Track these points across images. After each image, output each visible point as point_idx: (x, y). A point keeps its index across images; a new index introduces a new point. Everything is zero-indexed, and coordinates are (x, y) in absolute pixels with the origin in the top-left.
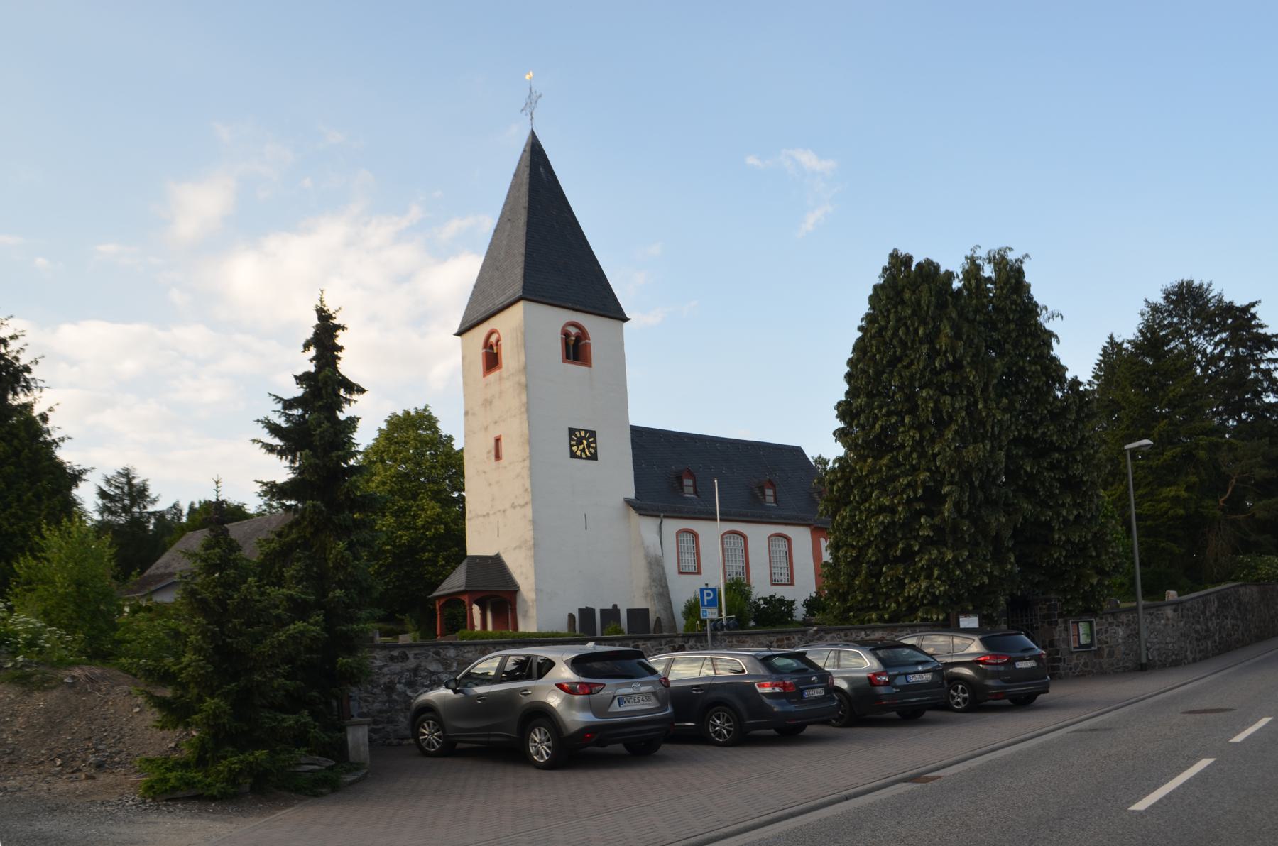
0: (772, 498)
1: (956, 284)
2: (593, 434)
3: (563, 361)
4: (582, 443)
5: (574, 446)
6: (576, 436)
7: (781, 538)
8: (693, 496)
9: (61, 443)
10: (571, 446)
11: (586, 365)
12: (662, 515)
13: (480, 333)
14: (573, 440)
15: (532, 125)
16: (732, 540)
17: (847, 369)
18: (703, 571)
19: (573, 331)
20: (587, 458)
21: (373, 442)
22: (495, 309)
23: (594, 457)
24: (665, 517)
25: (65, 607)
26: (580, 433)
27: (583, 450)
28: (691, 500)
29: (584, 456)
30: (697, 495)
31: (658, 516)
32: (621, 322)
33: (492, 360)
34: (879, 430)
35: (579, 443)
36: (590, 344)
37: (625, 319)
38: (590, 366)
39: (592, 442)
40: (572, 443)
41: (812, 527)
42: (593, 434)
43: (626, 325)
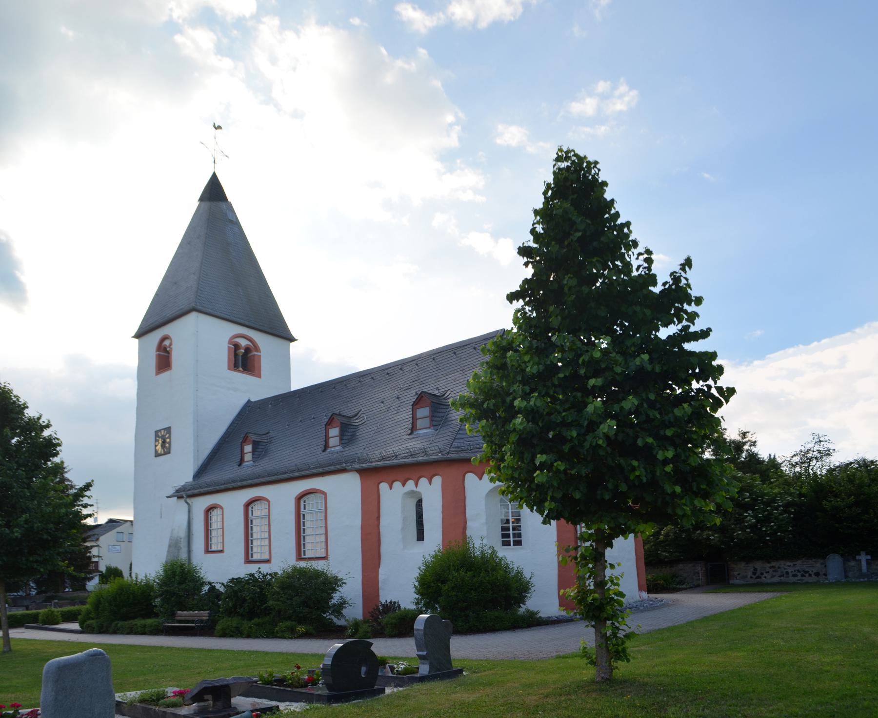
1: (683, 344)
9: (554, 162)
10: (156, 446)
11: (253, 375)
13: (155, 338)
21: (766, 458)
22: (157, 323)
32: (289, 342)
33: (164, 361)
34: (549, 492)
36: (260, 356)
37: (292, 339)
38: (259, 376)
43: (292, 344)
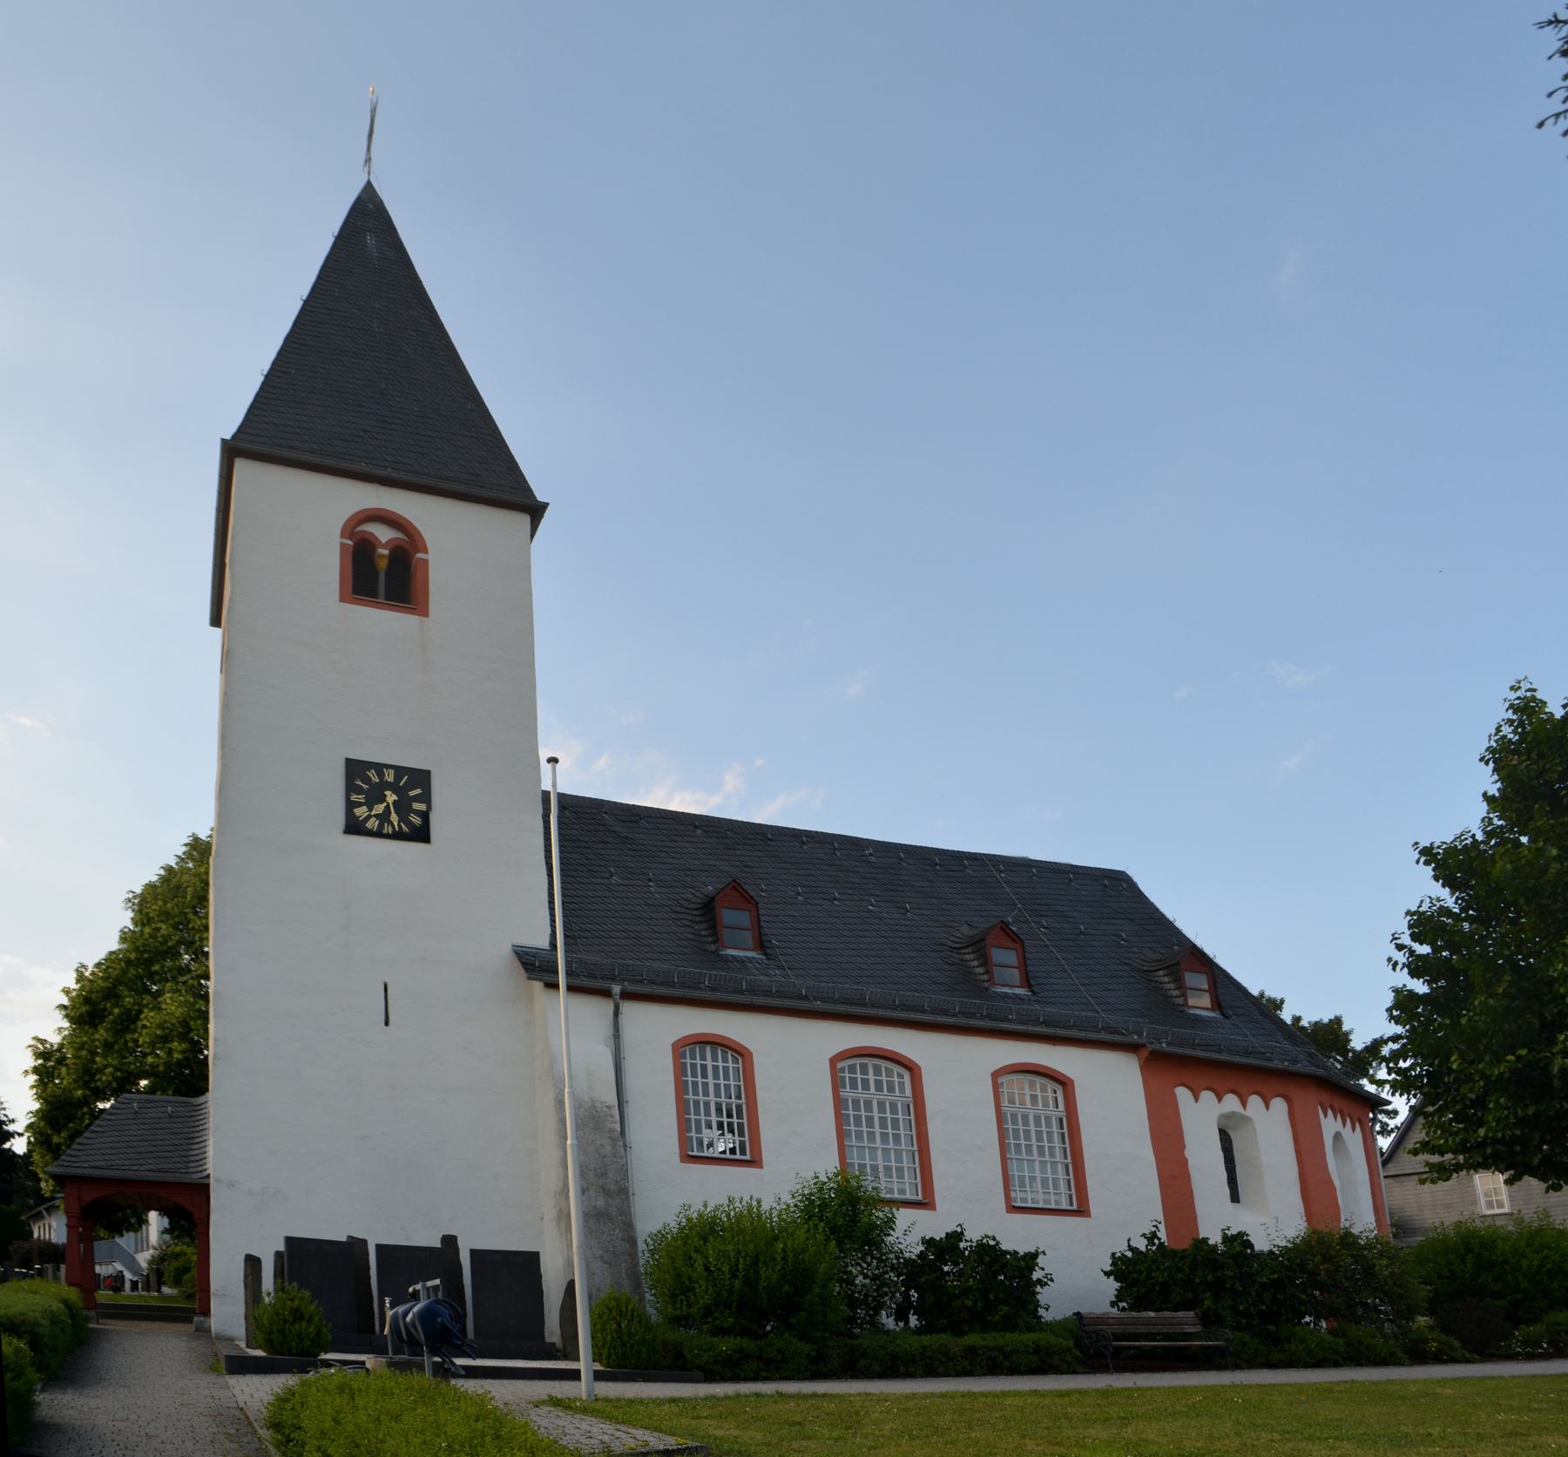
0: (1016, 973)
2: (421, 778)
3: (343, 599)
4: (383, 799)
5: (360, 805)
6: (367, 780)
7: (1038, 1080)
8: (750, 954)
12: (617, 989)
14: (359, 791)
15: (369, 173)
16: (871, 1077)
17: (1332, 1018)
18: (1093, 1209)
19: (383, 534)
20: (398, 836)
23: (421, 834)
24: (627, 996)
25: (853, 1231)
26: (381, 775)
27: (384, 818)
28: (743, 962)
29: (387, 829)
30: (765, 954)
31: (606, 994)
35: (375, 796)
36: (426, 561)
39: (417, 799)
40: (354, 797)
41: (1145, 1053)
42: (421, 778)
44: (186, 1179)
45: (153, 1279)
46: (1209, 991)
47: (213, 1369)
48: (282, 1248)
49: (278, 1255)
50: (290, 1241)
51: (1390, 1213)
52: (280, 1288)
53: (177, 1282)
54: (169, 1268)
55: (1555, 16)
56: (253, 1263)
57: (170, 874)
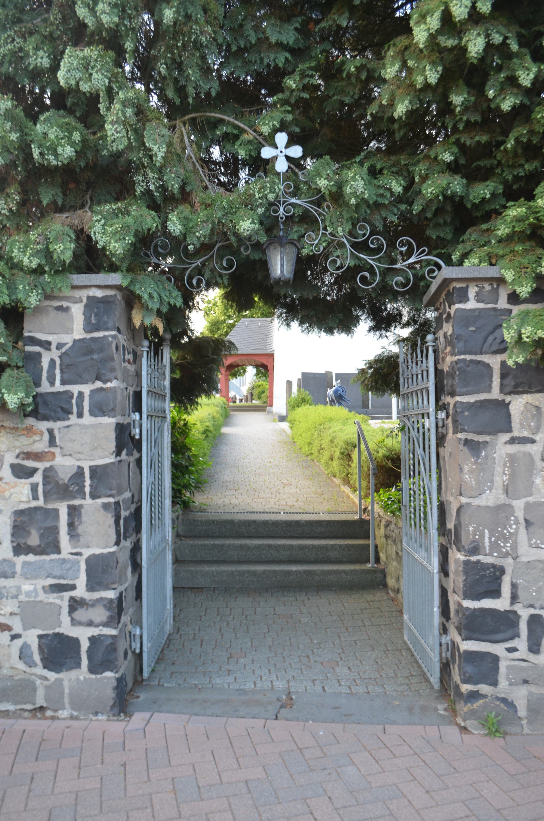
44: (265, 352)
45: (249, 397)
46: (228, 717)
47: (274, 421)
48: (300, 377)
49: (299, 380)
50: (304, 374)
51: (478, 443)
52: (299, 391)
53: (259, 398)
54: (256, 392)
55: (122, 765)
56: (289, 383)
57: (305, 112)
